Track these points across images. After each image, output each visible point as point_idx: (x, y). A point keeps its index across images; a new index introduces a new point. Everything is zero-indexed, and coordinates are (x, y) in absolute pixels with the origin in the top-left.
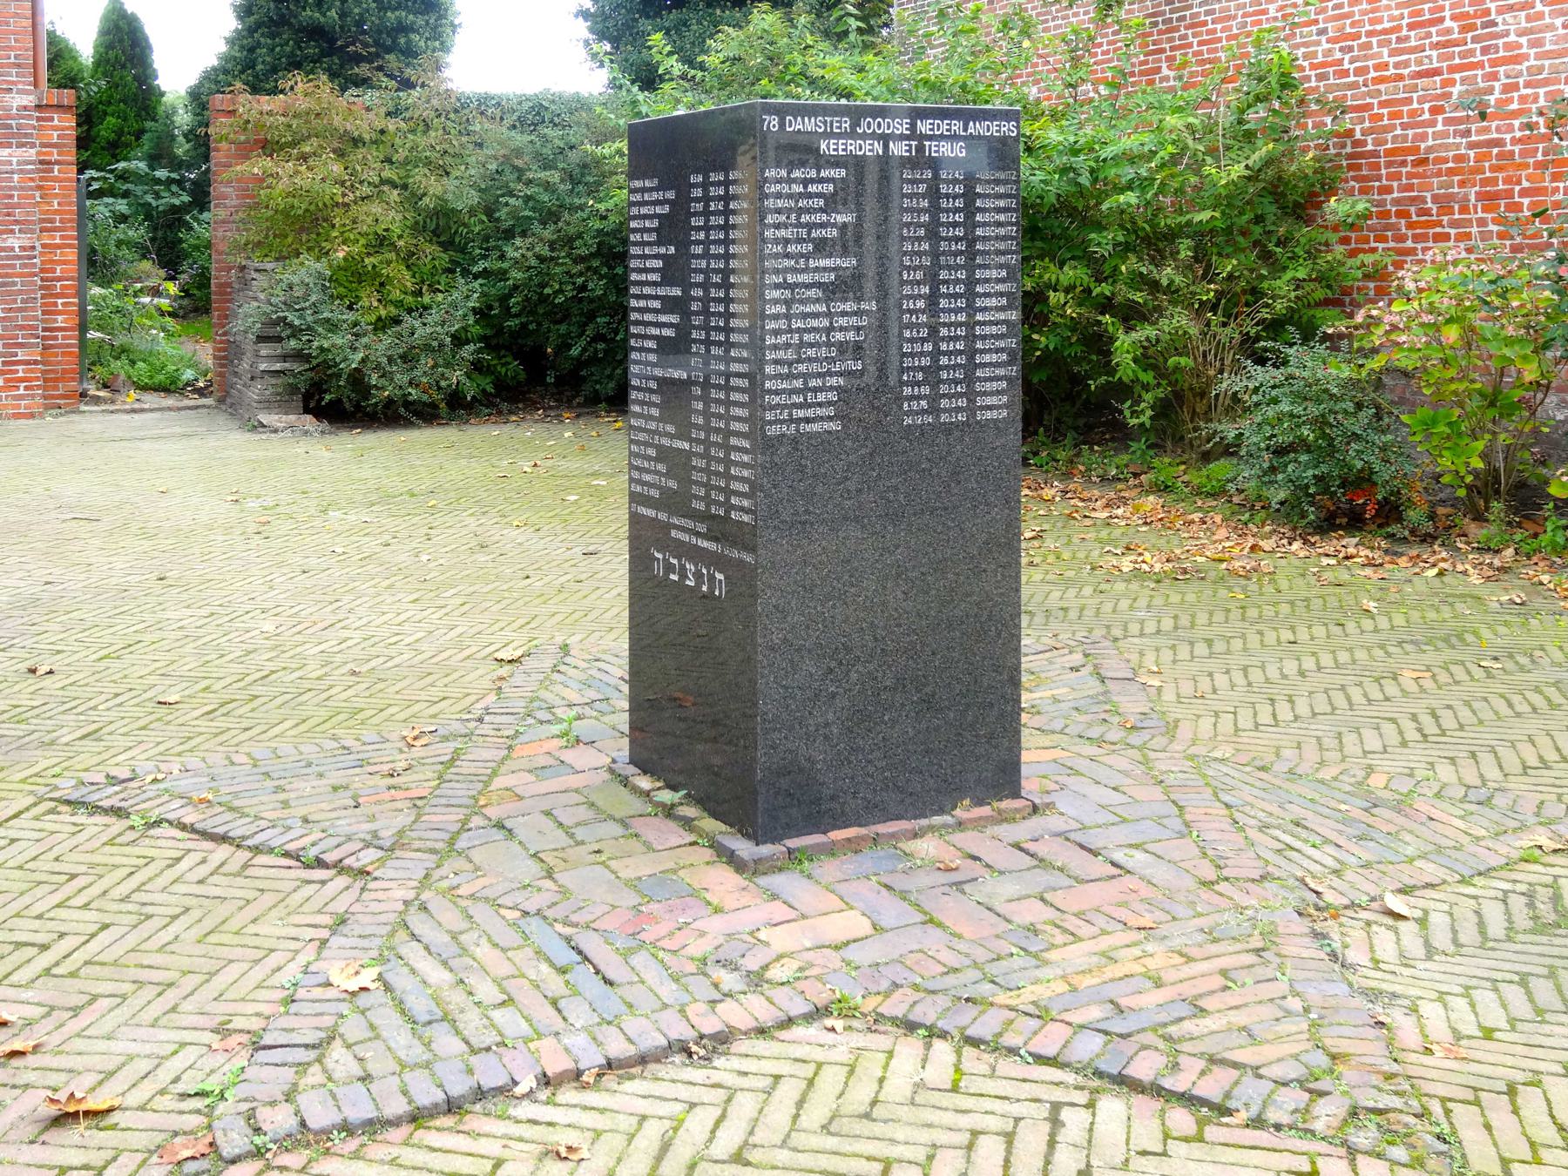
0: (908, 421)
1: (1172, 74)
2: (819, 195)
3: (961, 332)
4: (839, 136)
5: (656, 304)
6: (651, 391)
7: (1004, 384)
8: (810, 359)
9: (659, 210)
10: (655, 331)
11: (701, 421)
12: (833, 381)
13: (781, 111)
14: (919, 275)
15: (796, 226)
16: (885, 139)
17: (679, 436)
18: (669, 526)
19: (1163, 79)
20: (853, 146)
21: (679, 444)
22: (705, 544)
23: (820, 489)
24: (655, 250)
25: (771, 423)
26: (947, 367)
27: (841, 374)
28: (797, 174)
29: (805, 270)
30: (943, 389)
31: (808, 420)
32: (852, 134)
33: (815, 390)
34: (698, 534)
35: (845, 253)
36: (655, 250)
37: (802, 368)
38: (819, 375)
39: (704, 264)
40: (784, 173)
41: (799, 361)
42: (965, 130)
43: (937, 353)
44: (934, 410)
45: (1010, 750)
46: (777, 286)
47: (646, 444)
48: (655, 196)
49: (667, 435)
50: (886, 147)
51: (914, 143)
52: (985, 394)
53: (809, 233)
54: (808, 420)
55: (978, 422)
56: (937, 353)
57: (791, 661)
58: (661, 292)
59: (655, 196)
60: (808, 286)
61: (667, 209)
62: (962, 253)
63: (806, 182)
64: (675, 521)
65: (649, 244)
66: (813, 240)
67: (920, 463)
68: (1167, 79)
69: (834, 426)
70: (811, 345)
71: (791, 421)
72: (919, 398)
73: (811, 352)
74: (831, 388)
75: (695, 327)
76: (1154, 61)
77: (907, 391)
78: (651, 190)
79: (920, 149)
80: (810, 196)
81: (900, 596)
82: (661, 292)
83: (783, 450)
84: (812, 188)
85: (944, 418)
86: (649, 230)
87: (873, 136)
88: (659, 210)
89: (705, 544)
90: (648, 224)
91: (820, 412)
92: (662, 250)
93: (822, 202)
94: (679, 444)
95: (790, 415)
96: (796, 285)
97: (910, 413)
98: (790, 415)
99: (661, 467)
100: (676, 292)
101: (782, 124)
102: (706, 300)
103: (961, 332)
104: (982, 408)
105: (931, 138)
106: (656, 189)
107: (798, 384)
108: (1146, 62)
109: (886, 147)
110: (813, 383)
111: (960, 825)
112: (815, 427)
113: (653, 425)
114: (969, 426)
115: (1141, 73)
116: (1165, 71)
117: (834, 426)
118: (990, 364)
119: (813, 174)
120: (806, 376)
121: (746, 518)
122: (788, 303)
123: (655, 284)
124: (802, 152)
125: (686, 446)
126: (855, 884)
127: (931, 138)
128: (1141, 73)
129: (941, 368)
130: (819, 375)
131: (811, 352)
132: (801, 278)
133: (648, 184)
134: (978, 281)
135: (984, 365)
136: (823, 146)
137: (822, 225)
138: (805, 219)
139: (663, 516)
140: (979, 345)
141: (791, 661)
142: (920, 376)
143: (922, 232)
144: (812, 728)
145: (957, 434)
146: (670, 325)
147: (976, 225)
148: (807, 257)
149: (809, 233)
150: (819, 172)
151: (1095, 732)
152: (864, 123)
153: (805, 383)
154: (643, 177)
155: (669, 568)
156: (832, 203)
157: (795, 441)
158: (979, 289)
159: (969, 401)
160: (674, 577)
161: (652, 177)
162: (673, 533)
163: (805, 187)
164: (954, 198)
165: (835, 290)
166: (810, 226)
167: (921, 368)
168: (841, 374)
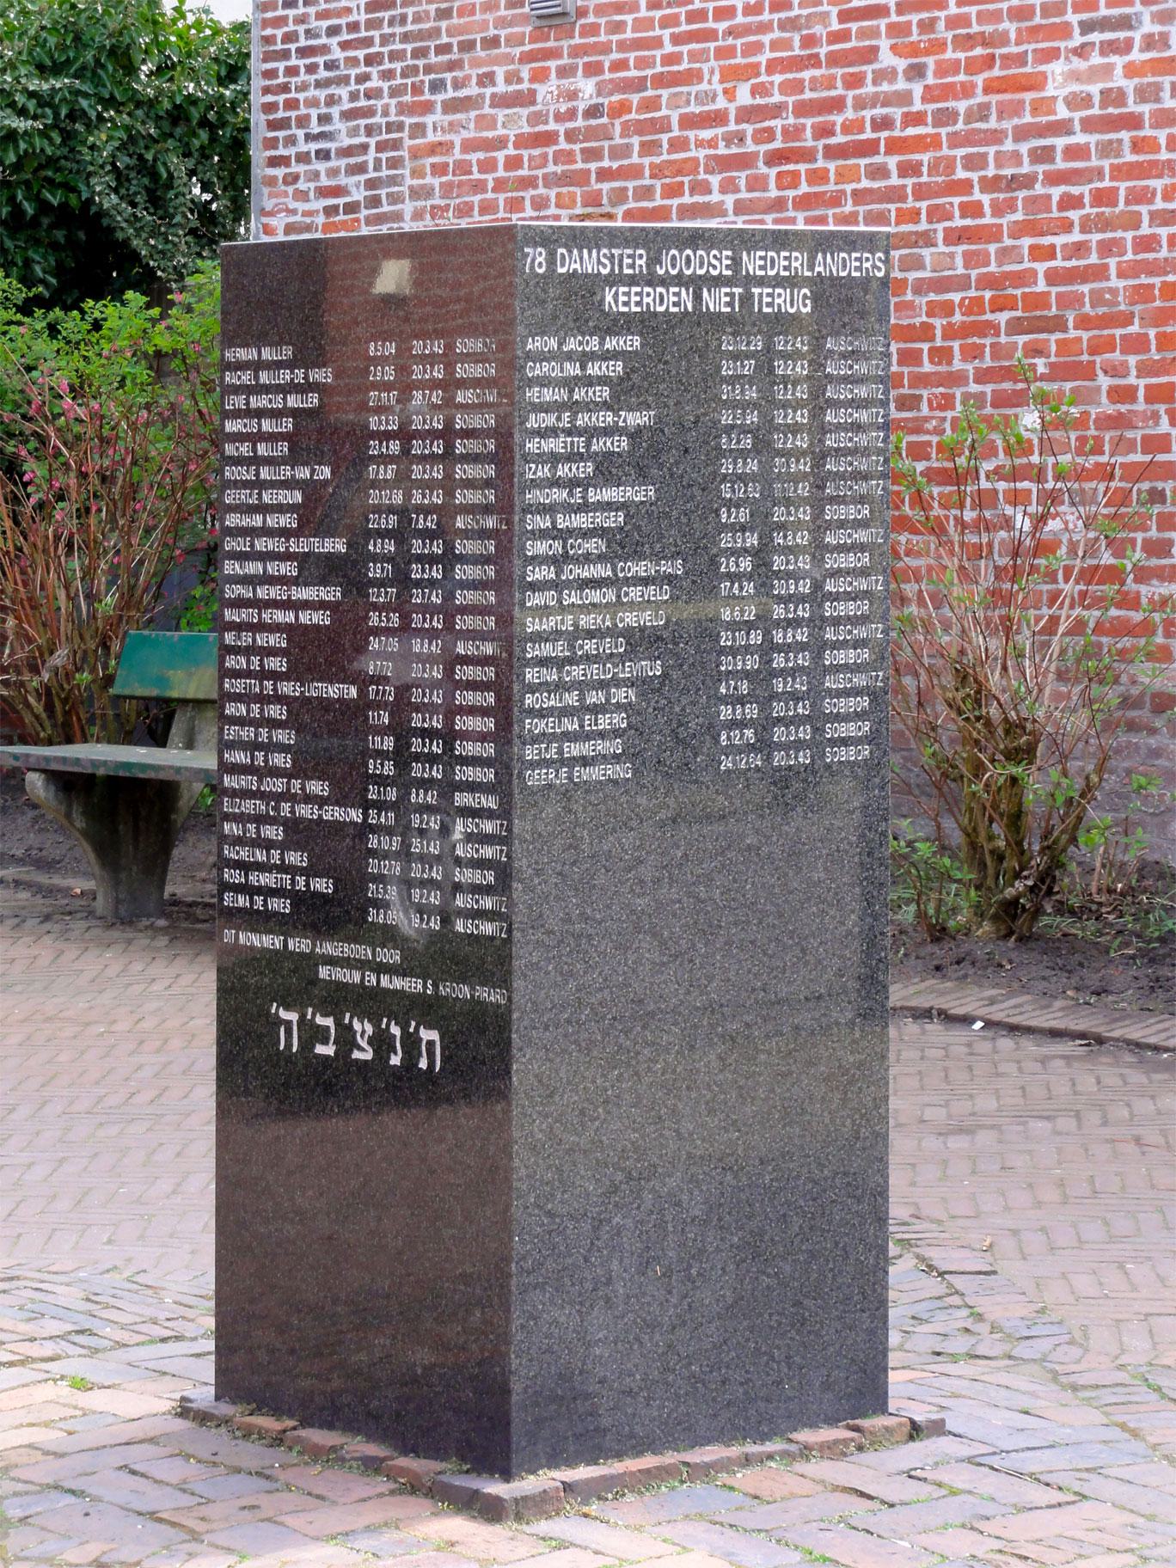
0: (727, 764)
1: (901, 64)
2: (603, 380)
3: (804, 612)
4: (632, 281)
5: (288, 569)
6: (274, 724)
7: (865, 702)
8: (588, 659)
9: (293, 401)
10: (284, 617)
11: (389, 769)
12: (620, 695)
13: (549, 239)
14: (743, 515)
15: (569, 433)
16: (696, 284)
17: (340, 800)
18: (312, 960)
19: (879, 77)
20: (651, 299)
21: (333, 813)
22: (398, 983)
23: (600, 880)
24: (286, 472)
25: (533, 765)
26: (782, 673)
27: (630, 683)
28: (572, 345)
29: (584, 507)
30: (778, 709)
31: (585, 761)
32: (652, 280)
33: (596, 710)
34: (380, 969)
35: (643, 477)
36: (286, 472)
37: (577, 672)
38: (602, 685)
39: (398, 498)
40: (553, 343)
41: (571, 661)
42: (811, 267)
43: (768, 648)
44: (764, 745)
45: (872, 1332)
46: (543, 534)
47: (260, 820)
48: (285, 376)
49: (308, 799)
50: (698, 298)
51: (737, 291)
52: (838, 718)
53: (588, 445)
54: (585, 761)
55: (828, 767)
56: (768, 648)
57: (559, 1170)
58: (297, 546)
59: (285, 376)
60: (586, 534)
61: (313, 400)
62: (805, 476)
63: (585, 358)
64: (328, 948)
65: (269, 461)
66: (591, 456)
67: (742, 837)
68: (888, 74)
69: (622, 771)
70: (590, 634)
71: (562, 762)
72: (741, 724)
73: (590, 646)
74: (619, 707)
75: (375, 607)
76: (862, 34)
77: (726, 712)
78: (279, 365)
79: (747, 299)
80: (590, 382)
81: (715, 1064)
82: (297, 546)
83: (549, 811)
84: (594, 369)
85: (778, 759)
86: (272, 438)
87: (680, 280)
88: (293, 401)
89: (398, 983)
90: (267, 425)
91: (602, 746)
92: (303, 473)
93: (606, 393)
94: (333, 813)
95: (560, 752)
96: (570, 532)
97: (731, 750)
98: (560, 752)
99: (295, 858)
100: (338, 546)
101: (551, 261)
102: (400, 563)
103: (804, 612)
104: (833, 742)
105: (761, 281)
106: (291, 365)
107: (571, 699)
108: (843, 36)
109: (698, 298)
110: (594, 698)
111: (806, 1452)
112: (595, 773)
113: (277, 785)
114: (814, 773)
115: (834, 60)
116: (887, 59)
117: (622, 771)
118: (846, 668)
119: (593, 344)
120: (582, 686)
121: (488, 928)
122: (558, 561)
123: (285, 533)
124: (579, 304)
125: (355, 815)
126: (679, 1526)
127: (761, 281)
128: (834, 60)
129: (774, 674)
130: (602, 685)
131: (590, 646)
132: (581, 521)
133: (267, 354)
134: (829, 526)
135: (837, 669)
136: (609, 298)
137: (607, 432)
138: (582, 420)
139: (299, 944)
140: (829, 635)
141: (559, 1170)
142: (744, 687)
143: (748, 442)
144: (589, 1286)
145: (797, 785)
146: (321, 605)
147: (824, 429)
148: (585, 484)
149: (588, 445)
150: (602, 342)
151: (960, 1345)
152: (666, 259)
153: (582, 699)
154: (260, 340)
155: (315, 1034)
156: (623, 393)
157: (566, 794)
158: (829, 539)
159: (816, 730)
160: (327, 1050)
161: (278, 344)
162: (324, 972)
163: (583, 368)
164: (795, 383)
165: (622, 545)
166: (591, 433)
167: (746, 675)
168: (630, 683)
